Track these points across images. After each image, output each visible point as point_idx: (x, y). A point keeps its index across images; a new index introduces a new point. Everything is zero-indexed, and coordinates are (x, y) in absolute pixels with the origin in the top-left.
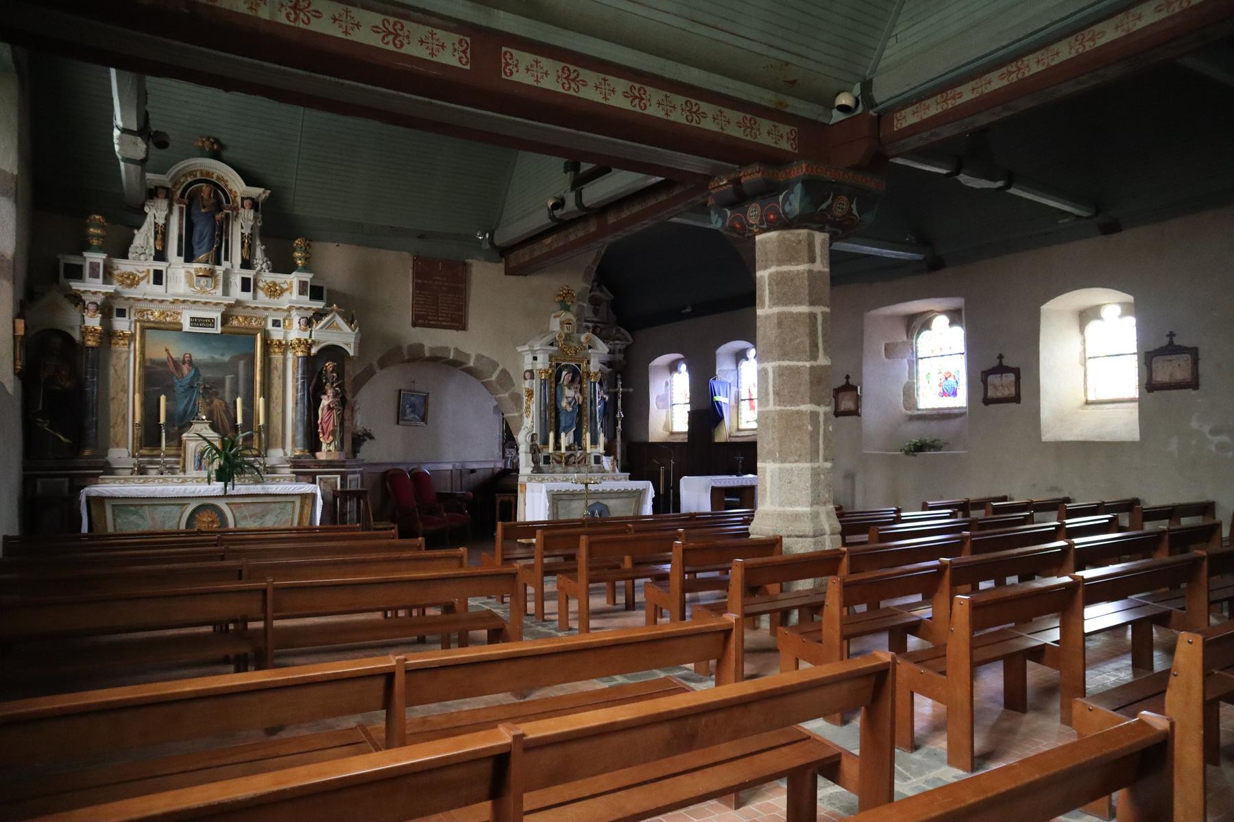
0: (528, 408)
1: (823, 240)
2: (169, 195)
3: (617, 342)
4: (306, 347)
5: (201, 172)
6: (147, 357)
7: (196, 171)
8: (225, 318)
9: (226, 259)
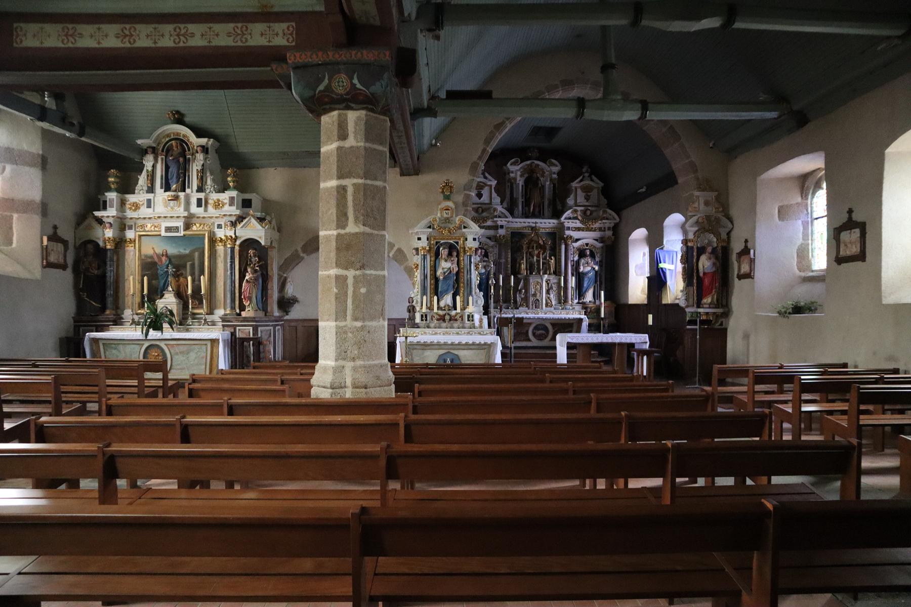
1: (359, 118)
2: (154, 150)
3: (604, 221)
4: (231, 241)
5: (174, 134)
6: (142, 253)
7: (170, 134)
8: (187, 226)
9: (189, 187)
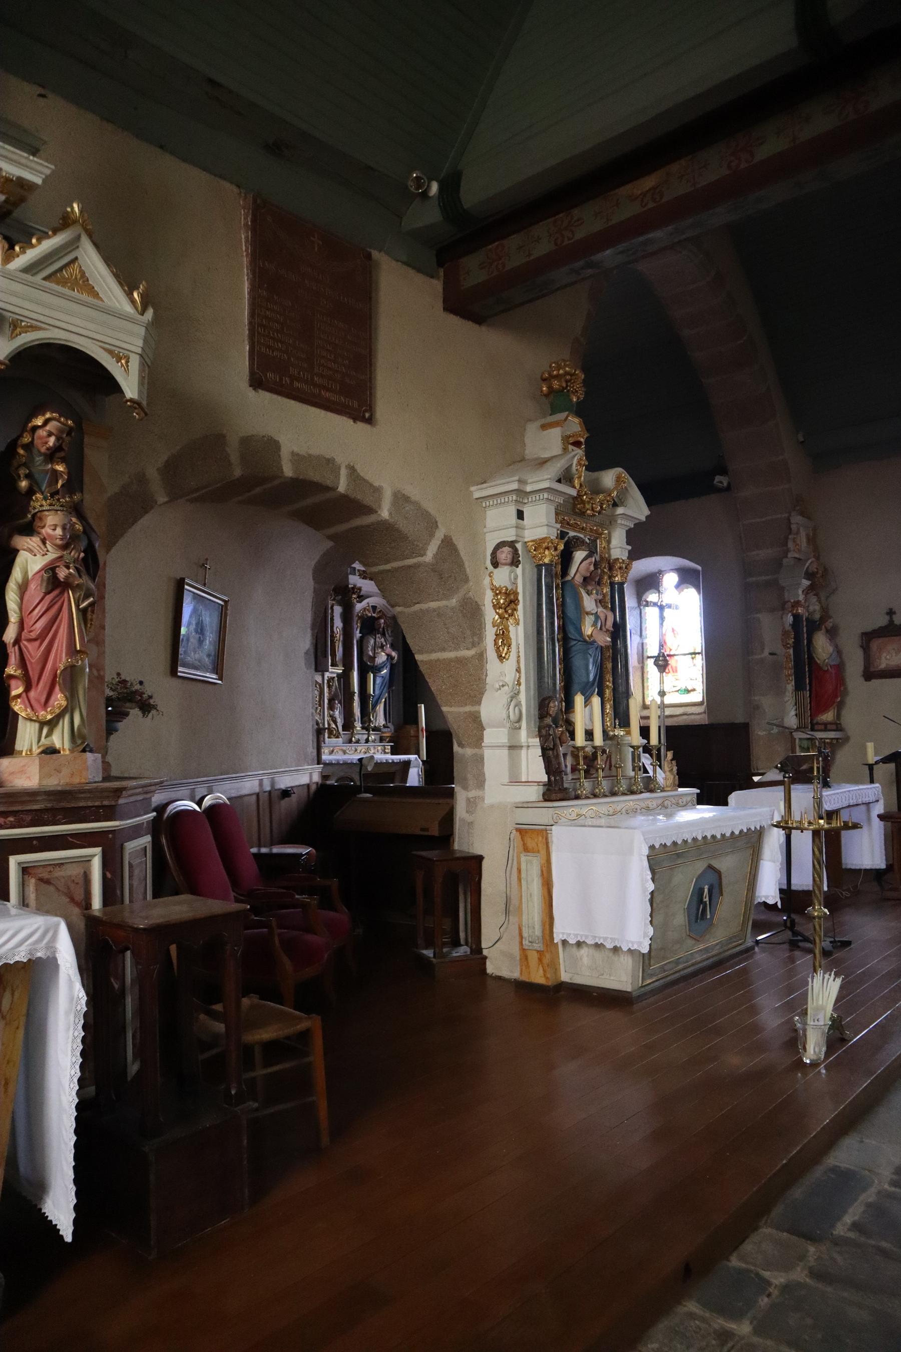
0: (503, 637)
